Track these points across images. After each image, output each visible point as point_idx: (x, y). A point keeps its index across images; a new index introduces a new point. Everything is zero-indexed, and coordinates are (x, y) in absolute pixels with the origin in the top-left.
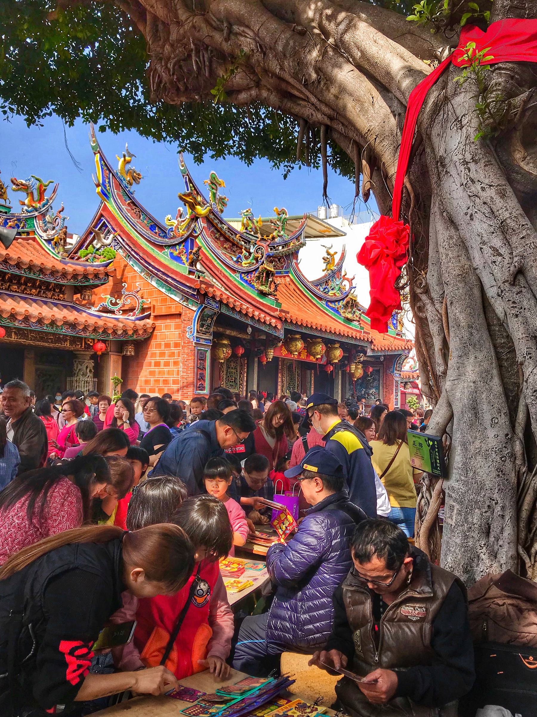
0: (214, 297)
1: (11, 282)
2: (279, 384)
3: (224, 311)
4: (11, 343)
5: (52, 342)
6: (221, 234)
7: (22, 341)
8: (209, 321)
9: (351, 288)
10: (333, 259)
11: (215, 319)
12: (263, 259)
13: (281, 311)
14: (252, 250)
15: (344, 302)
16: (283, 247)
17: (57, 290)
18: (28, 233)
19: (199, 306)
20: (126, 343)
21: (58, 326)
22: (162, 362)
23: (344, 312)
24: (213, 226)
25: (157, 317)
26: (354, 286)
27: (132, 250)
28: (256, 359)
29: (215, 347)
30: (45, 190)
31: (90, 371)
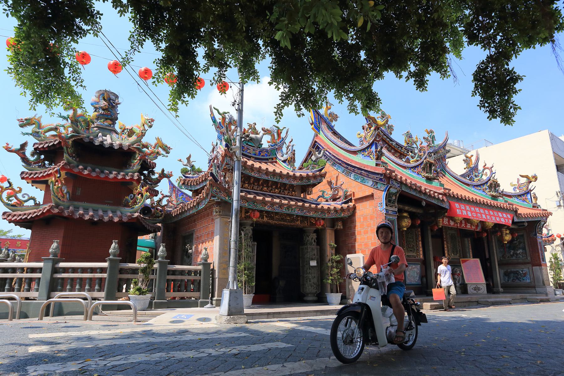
0: (396, 180)
1: (263, 186)
2: (446, 249)
3: (404, 189)
4: (264, 222)
5: (289, 222)
6: (392, 148)
7: (270, 221)
8: (394, 198)
9: (492, 173)
10: (471, 160)
11: (398, 195)
12: (426, 155)
13: (444, 189)
14: (416, 151)
15: (489, 184)
16: (434, 154)
17: (291, 190)
18: (272, 159)
19: (386, 186)
20: (337, 220)
21: (292, 209)
22: (362, 231)
23: (489, 192)
24: (386, 143)
25: (356, 200)
26: (494, 172)
27: (336, 158)
28: (429, 228)
29: (400, 218)
30: (281, 132)
31: (314, 241)
